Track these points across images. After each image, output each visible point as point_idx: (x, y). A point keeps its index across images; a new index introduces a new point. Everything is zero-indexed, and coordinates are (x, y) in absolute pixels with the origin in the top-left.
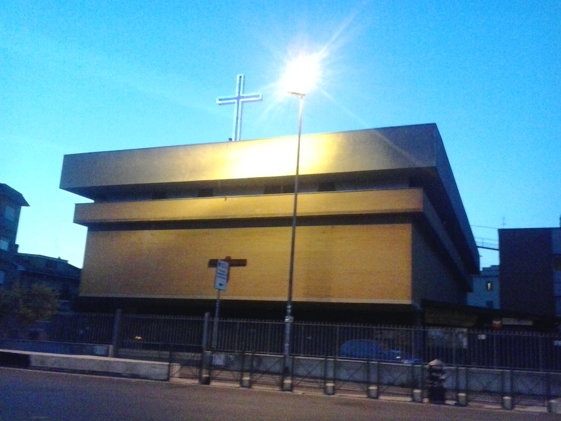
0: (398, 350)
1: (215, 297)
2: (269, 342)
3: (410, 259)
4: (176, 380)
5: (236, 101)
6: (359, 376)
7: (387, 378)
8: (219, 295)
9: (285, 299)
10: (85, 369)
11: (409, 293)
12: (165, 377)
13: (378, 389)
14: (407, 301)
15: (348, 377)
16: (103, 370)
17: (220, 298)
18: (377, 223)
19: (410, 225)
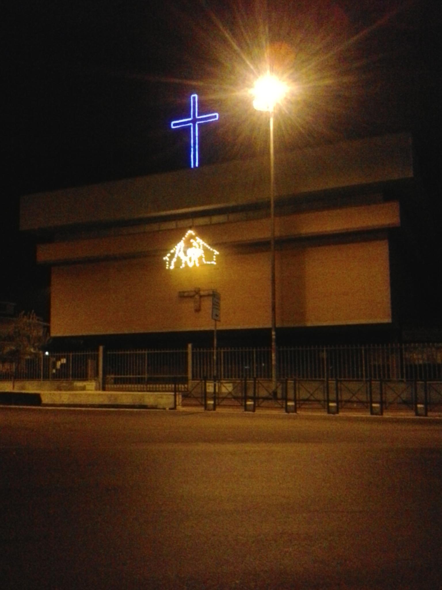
0: (110, 354)
1: (212, 328)
2: (215, 366)
3: (388, 278)
4: (180, 408)
5: (191, 124)
7: (345, 396)
8: (216, 325)
9: (269, 325)
10: (94, 403)
11: (389, 311)
12: (172, 406)
13: (254, 405)
14: (388, 320)
15: (309, 395)
16: (110, 403)
17: (218, 329)
18: (352, 242)
19: (386, 241)
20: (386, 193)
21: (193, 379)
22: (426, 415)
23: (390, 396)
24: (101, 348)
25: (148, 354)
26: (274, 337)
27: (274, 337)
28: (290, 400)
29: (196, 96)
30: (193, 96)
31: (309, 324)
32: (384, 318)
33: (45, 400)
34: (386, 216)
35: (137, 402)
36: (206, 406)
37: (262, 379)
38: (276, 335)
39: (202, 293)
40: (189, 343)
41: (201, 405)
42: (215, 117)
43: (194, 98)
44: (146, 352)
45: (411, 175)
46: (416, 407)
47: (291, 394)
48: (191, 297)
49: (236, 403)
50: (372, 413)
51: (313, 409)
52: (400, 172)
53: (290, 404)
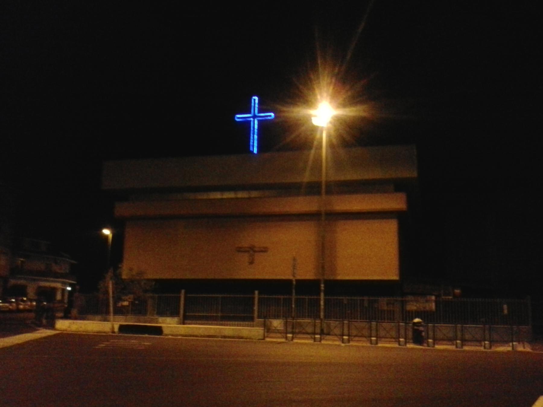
5: (252, 119)
6: (451, 335)
11: (397, 272)
14: (395, 277)
20: (398, 186)
21: (259, 317)
22: (434, 347)
23: (439, 335)
24: (183, 291)
25: (308, 299)
26: (322, 288)
27: (322, 288)
28: (317, 334)
29: (256, 98)
30: (254, 98)
31: (339, 278)
32: (393, 275)
33: (166, 331)
34: (396, 202)
35: (236, 334)
36: (286, 338)
37: (359, 320)
38: (324, 287)
39: (256, 249)
40: (257, 290)
41: (283, 337)
42: (270, 116)
43: (255, 100)
44: (307, 297)
45: (415, 174)
46: (428, 342)
47: (346, 331)
48: (248, 251)
49: (394, 340)
50: (399, 345)
51: (390, 342)
52: (410, 173)
53: (345, 337)
